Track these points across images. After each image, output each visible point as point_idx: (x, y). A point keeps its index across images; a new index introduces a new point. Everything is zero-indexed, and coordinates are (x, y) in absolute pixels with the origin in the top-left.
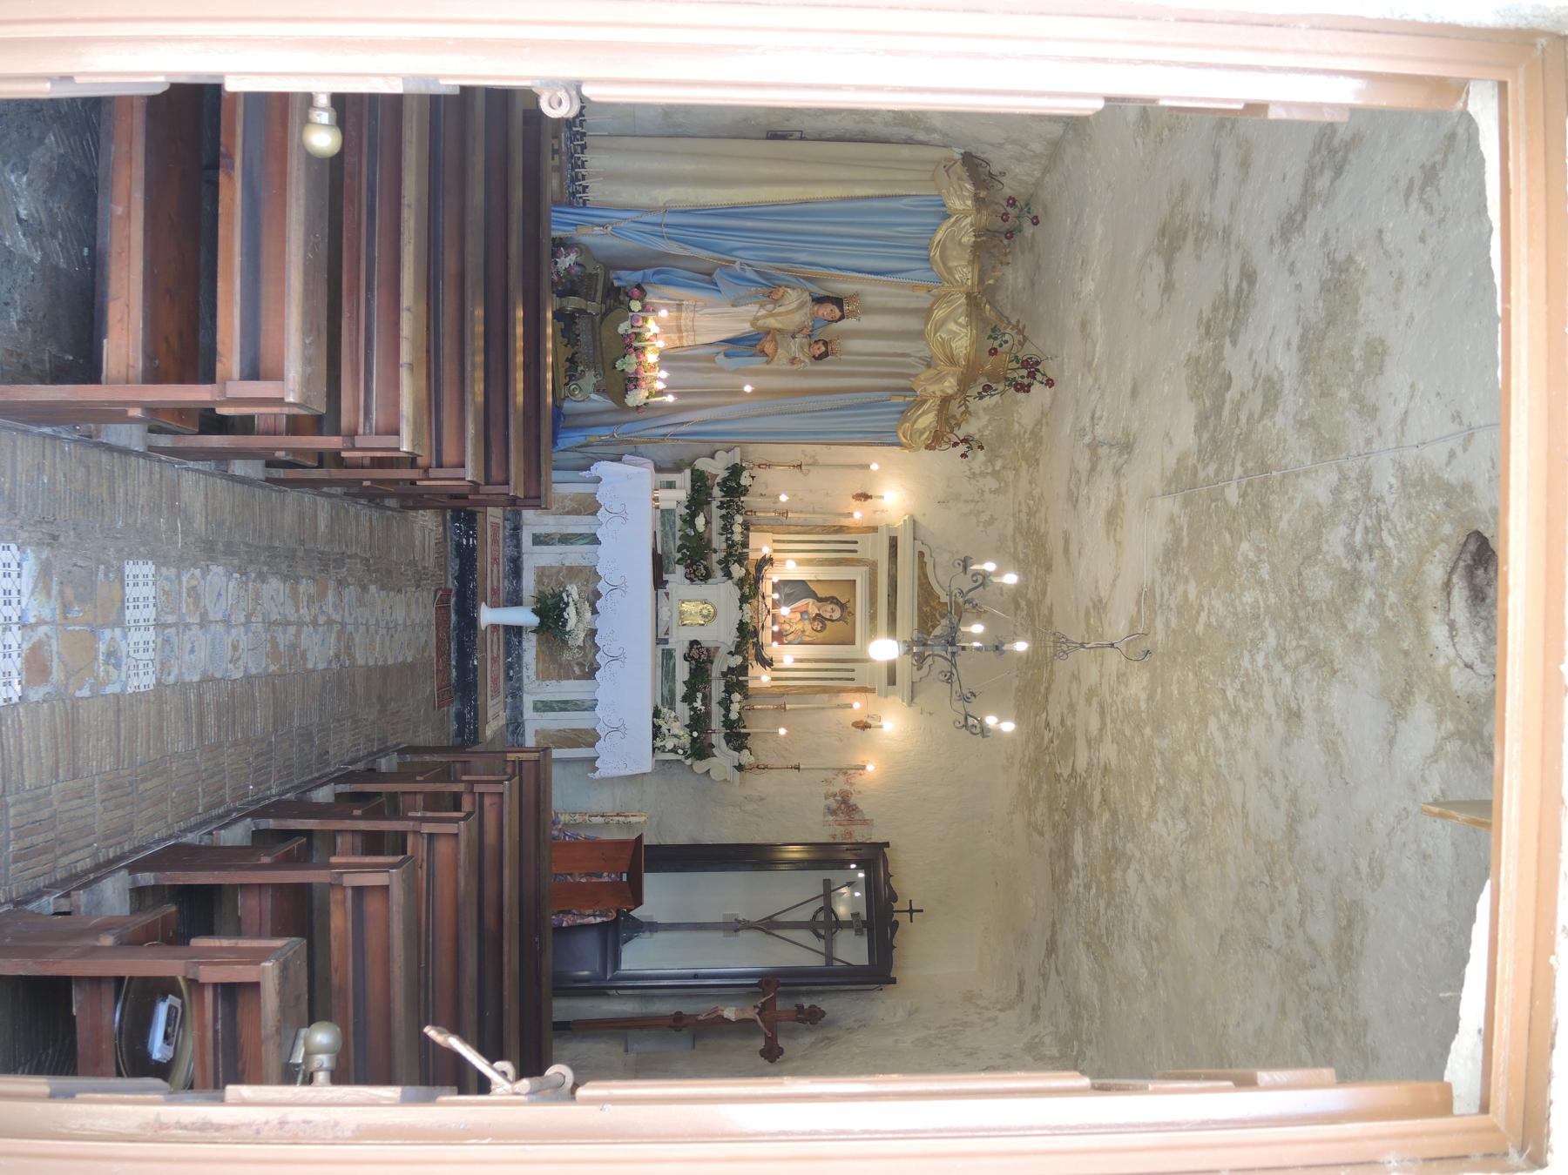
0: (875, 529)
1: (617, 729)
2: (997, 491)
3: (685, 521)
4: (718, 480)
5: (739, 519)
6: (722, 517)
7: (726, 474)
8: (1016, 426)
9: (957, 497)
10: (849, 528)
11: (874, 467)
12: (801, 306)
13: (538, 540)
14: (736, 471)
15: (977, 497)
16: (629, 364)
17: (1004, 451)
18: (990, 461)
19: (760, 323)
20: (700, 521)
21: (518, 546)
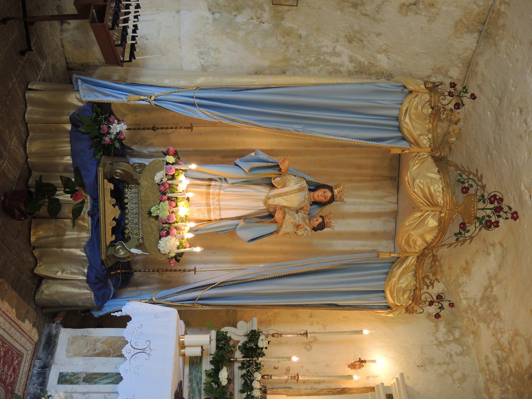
0: (372, 389)
1: (143, 351)
2: (462, 354)
3: (209, 375)
4: (240, 344)
5: (258, 376)
6: (243, 376)
7: (246, 339)
8: (464, 302)
9: (431, 361)
10: (350, 389)
11: (366, 332)
12: (301, 190)
13: (63, 379)
14: (254, 336)
15: (447, 360)
16: (163, 210)
17: (459, 323)
18: (450, 332)
19: (271, 202)
20: (223, 375)
21: (43, 384)
